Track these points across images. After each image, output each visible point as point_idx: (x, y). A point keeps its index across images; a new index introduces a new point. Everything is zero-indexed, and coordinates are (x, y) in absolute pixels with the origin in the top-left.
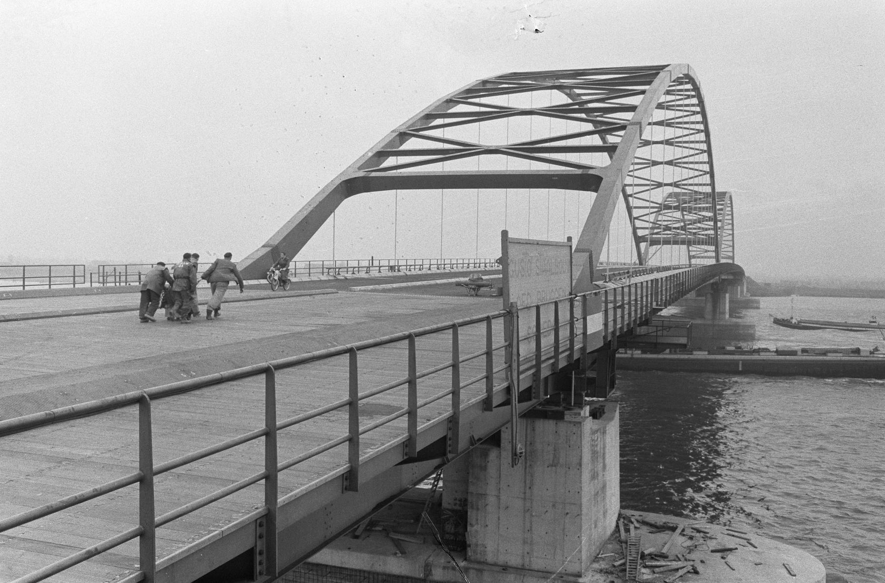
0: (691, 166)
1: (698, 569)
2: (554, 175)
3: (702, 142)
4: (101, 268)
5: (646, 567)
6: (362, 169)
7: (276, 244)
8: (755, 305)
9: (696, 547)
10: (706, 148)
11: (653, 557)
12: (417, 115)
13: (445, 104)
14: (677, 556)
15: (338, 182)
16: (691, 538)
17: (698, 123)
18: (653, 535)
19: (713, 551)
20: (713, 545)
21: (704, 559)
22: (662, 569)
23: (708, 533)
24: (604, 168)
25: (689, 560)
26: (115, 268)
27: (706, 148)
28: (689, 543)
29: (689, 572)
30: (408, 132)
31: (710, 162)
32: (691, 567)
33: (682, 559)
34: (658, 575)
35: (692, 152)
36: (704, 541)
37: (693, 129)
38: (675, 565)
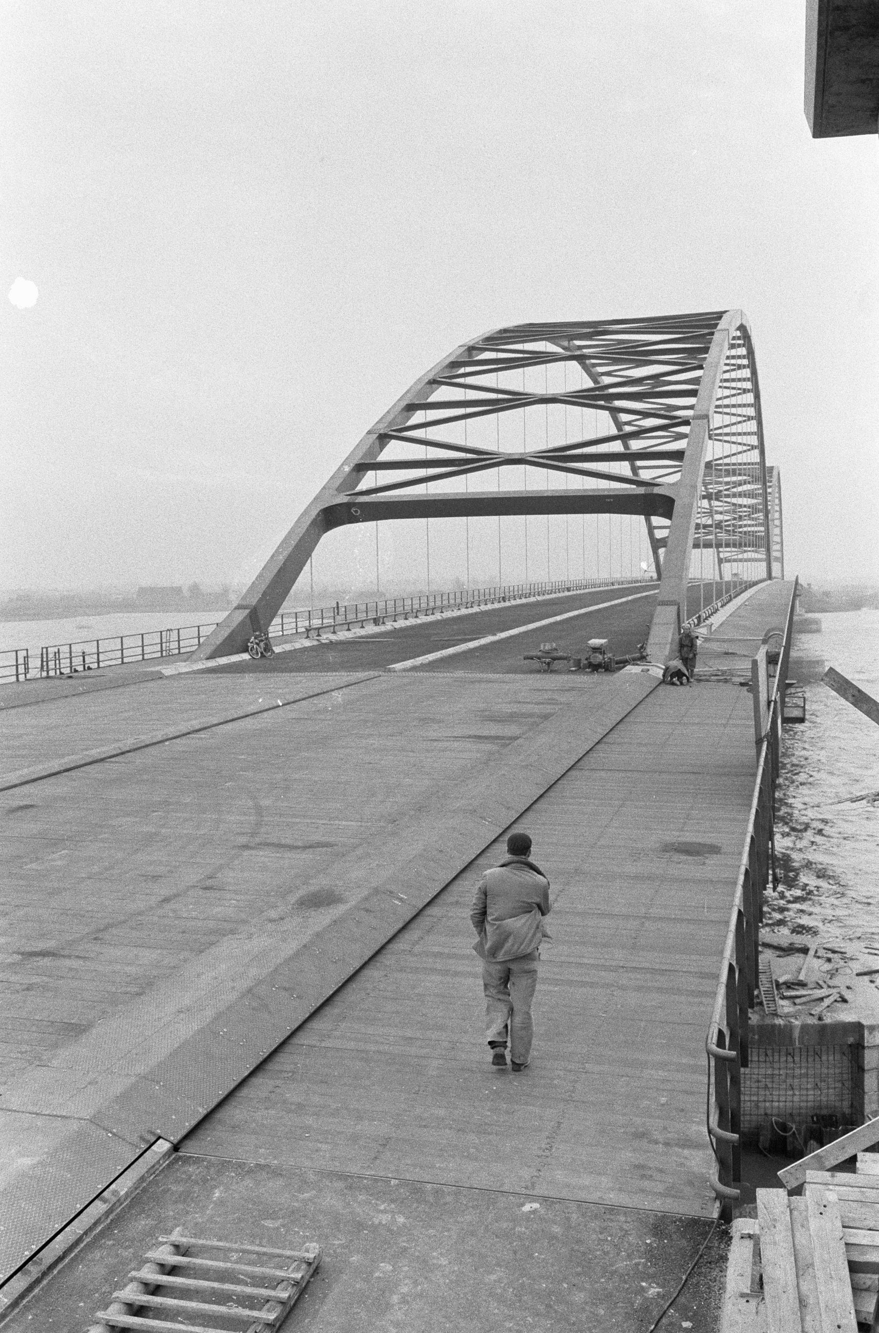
0: (734, 439)
1: (846, 997)
2: (609, 496)
3: (749, 405)
4: (45, 650)
5: (784, 998)
6: (343, 492)
7: (254, 604)
8: (814, 627)
9: (837, 971)
10: (756, 443)
11: (789, 985)
12: (393, 406)
13: (428, 386)
14: (818, 983)
15: (314, 513)
16: (829, 960)
17: (744, 380)
18: (781, 959)
19: (858, 975)
20: (857, 967)
21: (851, 986)
22: (803, 1000)
23: (845, 953)
24: (673, 484)
25: (834, 987)
26: (59, 649)
27: (756, 443)
28: (827, 967)
29: (836, 1001)
30: (390, 433)
31: (760, 434)
32: (839, 995)
33: (825, 986)
34: (800, 1007)
35: (734, 419)
36: (846, 962)
37: (734, 388)
38: (819, 993)
